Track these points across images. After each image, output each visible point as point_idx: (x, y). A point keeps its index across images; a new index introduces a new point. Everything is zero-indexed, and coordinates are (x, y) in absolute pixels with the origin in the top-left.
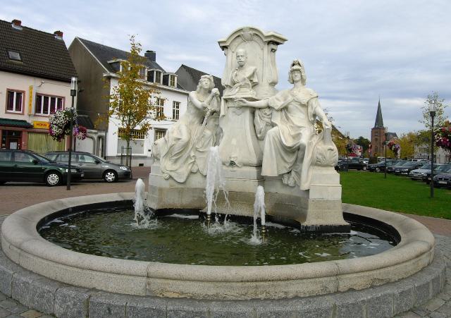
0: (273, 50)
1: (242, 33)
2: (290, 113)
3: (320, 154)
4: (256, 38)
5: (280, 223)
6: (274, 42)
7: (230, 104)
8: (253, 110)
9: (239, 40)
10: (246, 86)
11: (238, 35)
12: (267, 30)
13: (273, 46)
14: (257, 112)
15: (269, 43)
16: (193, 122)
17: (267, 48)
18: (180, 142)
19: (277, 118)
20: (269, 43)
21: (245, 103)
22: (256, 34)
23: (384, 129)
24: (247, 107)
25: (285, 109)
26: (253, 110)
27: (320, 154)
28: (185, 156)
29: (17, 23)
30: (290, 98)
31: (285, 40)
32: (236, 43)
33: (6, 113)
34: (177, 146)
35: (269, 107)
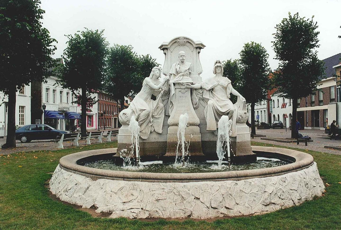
0: (199, 52)
1: (179, 40)
2: (214, 92)
3: (240, 116)
4: (188, 44)
5: (6, 108)
6: (200, 47)
7: (177, 86)
8: (192, 90)
9: (176, 44)
10: (187, 75)
11: (175, 41)
12: (196, 40)
13: (198, 50)
14: (194, 92)
15: (197, 48)
16: (147, 98)
17: (195, 52)
18: (144, 112)
19: (207, 95)
20: (197, 48)
21: (190, 86)
22: (188, 42)
23: (117, 51)
24: (189, 88)
25: (212, 90)
26: (192, 90)
27: (240, 116)
28: (148, 121)
29: (237, 102)
30: (216, 83)
31: (205, 46)
32: (173, 47)
33: (20, 107)
34: (141, 115)
35: (201, 88)
